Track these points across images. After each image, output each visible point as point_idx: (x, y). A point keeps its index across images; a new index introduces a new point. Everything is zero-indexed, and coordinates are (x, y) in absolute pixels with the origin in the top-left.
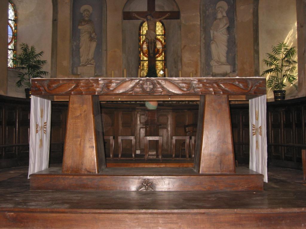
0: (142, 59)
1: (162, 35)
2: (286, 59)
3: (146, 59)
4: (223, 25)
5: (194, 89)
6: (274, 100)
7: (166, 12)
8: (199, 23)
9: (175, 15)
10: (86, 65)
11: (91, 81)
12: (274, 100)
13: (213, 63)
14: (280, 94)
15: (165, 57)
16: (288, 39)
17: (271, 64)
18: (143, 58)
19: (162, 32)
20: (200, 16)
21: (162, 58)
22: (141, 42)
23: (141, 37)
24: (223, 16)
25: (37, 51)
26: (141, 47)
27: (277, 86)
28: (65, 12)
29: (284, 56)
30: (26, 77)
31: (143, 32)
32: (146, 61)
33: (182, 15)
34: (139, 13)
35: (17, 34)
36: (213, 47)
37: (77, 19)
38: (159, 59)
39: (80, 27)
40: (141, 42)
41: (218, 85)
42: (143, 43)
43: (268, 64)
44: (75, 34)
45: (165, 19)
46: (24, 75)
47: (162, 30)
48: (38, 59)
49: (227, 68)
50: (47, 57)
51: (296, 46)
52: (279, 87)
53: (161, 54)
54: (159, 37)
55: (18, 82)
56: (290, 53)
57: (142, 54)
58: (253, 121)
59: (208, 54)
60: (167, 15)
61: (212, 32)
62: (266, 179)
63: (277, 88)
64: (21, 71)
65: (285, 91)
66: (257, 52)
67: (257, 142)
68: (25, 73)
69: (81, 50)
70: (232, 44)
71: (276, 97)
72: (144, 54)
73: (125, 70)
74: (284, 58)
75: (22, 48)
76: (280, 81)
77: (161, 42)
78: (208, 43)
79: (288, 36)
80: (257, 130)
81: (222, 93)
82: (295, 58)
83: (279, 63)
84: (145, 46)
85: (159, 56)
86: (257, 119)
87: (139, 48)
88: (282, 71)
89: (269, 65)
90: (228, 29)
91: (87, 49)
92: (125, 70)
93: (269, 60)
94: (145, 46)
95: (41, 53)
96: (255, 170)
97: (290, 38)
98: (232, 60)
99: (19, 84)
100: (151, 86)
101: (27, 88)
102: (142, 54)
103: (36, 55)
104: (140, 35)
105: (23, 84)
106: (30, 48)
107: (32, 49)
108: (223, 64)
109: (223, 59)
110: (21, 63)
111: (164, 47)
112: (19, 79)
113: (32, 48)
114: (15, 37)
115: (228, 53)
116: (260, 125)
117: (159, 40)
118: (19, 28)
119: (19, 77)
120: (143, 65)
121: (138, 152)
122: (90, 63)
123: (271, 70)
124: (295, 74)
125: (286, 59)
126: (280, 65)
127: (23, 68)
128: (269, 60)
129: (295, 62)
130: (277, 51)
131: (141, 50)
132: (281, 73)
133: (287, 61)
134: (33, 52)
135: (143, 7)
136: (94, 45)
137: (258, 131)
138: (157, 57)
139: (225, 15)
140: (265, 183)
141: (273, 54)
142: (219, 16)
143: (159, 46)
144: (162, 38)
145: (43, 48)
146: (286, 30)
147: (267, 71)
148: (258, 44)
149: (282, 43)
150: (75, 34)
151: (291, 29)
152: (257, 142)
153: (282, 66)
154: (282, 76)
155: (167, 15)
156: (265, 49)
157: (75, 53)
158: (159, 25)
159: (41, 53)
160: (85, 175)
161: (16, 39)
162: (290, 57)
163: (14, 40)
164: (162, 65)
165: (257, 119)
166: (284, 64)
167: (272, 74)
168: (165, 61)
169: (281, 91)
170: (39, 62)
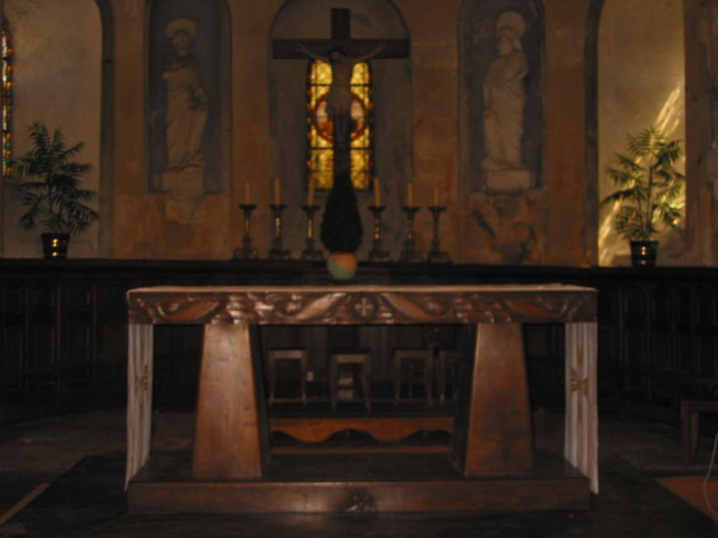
0: (313, 144)
1: (365, 85)
2: (660, 168)
3: (323, 143)
4: (514, 70)
5: (455, 312)
6: (628, 263)
7: (375, 42)
8: (455, 65)
9: (399, 49)
10: (182, 169)
11: (250, 296)
12: (628, 263)
13: (488, 164)
14: (643, 262)
15: (371, 139)
16: (668, 111)
17: (625, 178)
18: (317, 142)
19: (364, 78)
20: (459, 49)
21: (364, 142)
22: (313, 103)
23: (313, 89)
24: (515, 51)
25: (69, 143)
26: (312, 114)
27: (637, 231)
28: (132, 41)
29: (655, 161)
30: (45, 204)
31: (316, 78)
32: (325, 149)
33: (414, 44)
34: (310, 43)
35: (12, 93)
36: (489, 126)
37: (159, 55)
38: (356, 143)
39: (166, 76)
40: (313, 103)
41: (503, 305)
42: (319, 102)
43: (616, 179)
44: (156, 91)
45: (375, 57)
46: (39, 200)
47: (363, 74)
48: (70, 160)
49: (522, 178)
50: (90, 155)
51: (682, 136)
52: (642, 234)
53: (361, 133)
54: (356, 90)
55: (25, 217)
56: (667, 154)
57: (314, 132)
58: (572, 361)
59: (477, 137)
60: (379, 49)
61: (485, 89)
62: (595, 487)
63: (639, 237)
64: (33, 191)
65: (656, 243)
66: (593, 143)
67: (580, 407)
68: (41, 195)
69: (170, 131)
70: (533, 116)
71: (635, 256)
72: (320, 133)
73: (277, 183)
74: (656, 166)
75: (34, 134)
76: (644, 220)
77: (361, 102)
78: (476, 114)
79: (667, 105)
80: (580, 383)
81: (509, 319)
82: (680, 165)
83: (643, 175)
84: (322, 113)
85: (357, 137)
86: (580, 361)
87: (308, 116)
88: (649, 195)
89: (619, 180)
90: (527, 81)
91: (185, 129)
92: (277, 183)
93: (621, 168)
94: (322, 113)
95: (78, 148)
96: (575, 463)
97: (668, 117)
98: (533, 157)
99: (28, 221)
100: (370, 307)
101: (46, 232)
102: (314, 132)
103: (67, 152)
104: (309, 84)
105: (36, 221)
106: (51, 134)
107: (55, 136)
108: (511, 167)
109: (513, 154)
110: (31, 170)
111: (370, 114)
112: (26, 210)
113: (57, 134)
114: (9, 100)
115: (523, 140)
116: (585, 376)
117: (356, 97)
118: (18, 76)
119: (26, 204)
120: (317, 160)
121: (310, 377)
122: (191, 162)
123: (627, 194)
124: (679, 203)
125: (660, 168)
126: (646, 180)
127: (37, 185)
128: (621, 168)
129: (679, 176)
130: (639, 145)
131: (312, 121)
132: (648, 201)
133: (663, 173)
134: (58, 147)
135: (322, 29)
136: (201, 118)
137: (580, 385)
138: (353, 140)
139: (518, 45)
140: (592, 494)
141: (628, 154)
142: (505, 49)
143: (357, 113)
144: (364, 92)
145: (82, 134)
146: (662, 91)
147: (616, 196)
148: (595, 126)
149: (649, 130)
150: (156, 91)
151: (674, 88)
152: (580, 407)
153: (651, 184)
154: (650, 208)
155: (379, 49)
156: (610, 148)
157: (157, 134)
158: (359, 75)
159: (78, 148)
160: (238, 481)
161: (11, 104)
162: (669, 163)
163: (7, 108)
164: (364, 159)
165: (580, 361)
166: (655, 180)
167: (628, 202)
168: (371, 150)
169: (647, 244)
170: (74, 167)
